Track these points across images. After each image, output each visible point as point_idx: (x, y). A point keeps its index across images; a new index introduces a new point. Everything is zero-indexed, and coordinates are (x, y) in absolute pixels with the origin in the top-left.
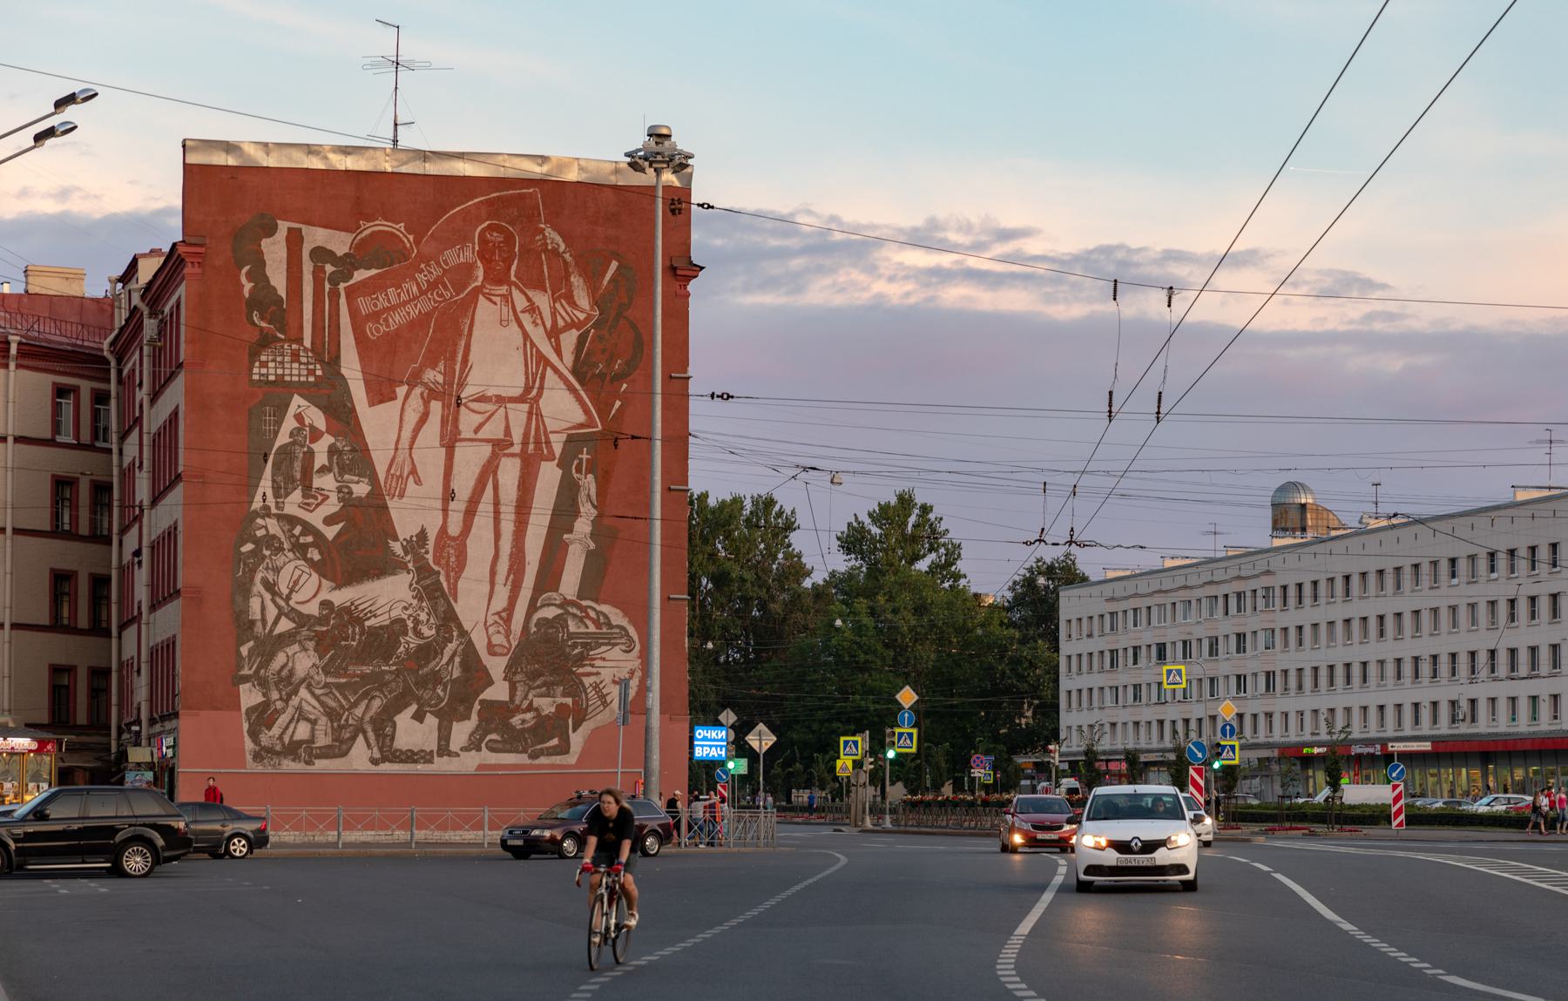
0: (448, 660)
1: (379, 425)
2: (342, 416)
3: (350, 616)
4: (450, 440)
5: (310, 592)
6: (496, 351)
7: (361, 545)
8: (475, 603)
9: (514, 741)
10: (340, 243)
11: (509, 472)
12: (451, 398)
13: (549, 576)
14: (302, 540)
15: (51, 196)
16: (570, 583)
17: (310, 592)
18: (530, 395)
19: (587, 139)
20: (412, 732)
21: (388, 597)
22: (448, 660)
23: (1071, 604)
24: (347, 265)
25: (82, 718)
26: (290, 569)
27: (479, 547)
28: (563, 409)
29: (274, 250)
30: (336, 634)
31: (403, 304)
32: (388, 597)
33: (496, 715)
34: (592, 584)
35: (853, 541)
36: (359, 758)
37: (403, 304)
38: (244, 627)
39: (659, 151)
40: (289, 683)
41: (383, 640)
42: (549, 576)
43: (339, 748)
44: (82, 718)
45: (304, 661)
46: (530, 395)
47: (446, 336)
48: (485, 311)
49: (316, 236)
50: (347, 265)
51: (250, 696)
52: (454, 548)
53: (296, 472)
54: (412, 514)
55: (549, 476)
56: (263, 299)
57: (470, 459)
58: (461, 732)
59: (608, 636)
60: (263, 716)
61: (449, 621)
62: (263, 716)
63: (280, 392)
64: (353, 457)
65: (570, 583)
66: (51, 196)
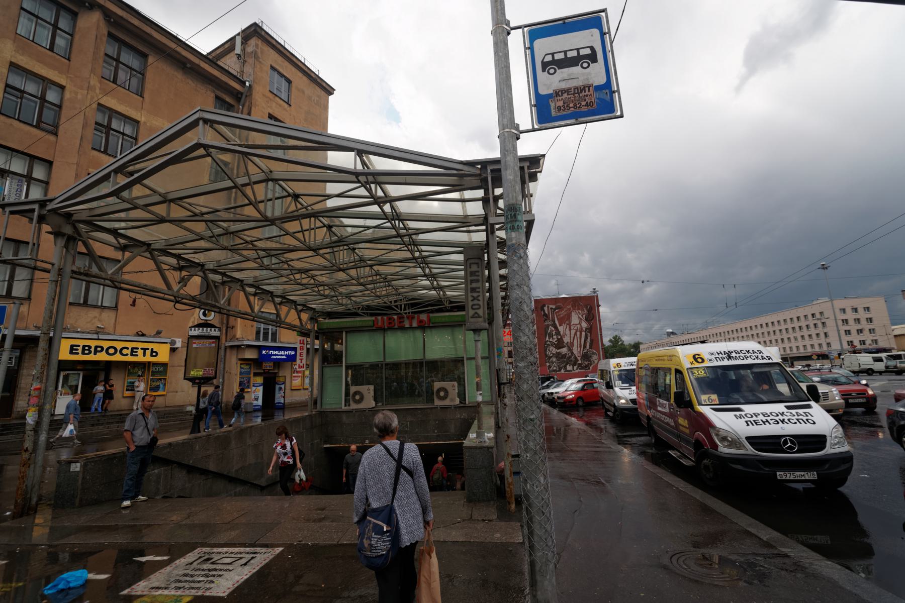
0: (573, 358)
1: (561, 329)
2: (556, 328)
3: (559, 353)
4: (570, 330)
5: (554, 351)
6: (575, 319)
7: (560, 344)
8: (576, 350)
9: (582, 368)
10: (554, 307)
11: (578, 333)
12: (569, 324)
13: (585, 347)
14: (552, 344)
15: (744, 80)
16: (588, 347)
17: (554, 351)
18: (580, 324)
19: (585, 292)
20: (569, 368)
21: (564, 350)
22: (573, 358)
23: (641, 347)
24: (555, 309)
25: (293, 353)
26: (551, 348)
27: (575, 343)
28: (584, 325)
29: (546, 308)
30: (558, 355)
31: (563, 313)
32: (564, 350)
33: (580, 365)
34: (591, 347)
35: (610, 341)
36: (563, 371)
37: (563, 313)
38: (546, 355)
39: (594, 291)
40: (552, 362)
41: (564, 356)
42: (585, 347)
43: (560, 370)
44: (293, 353)
45: (554, 360)
46: (580, 324)
47: (568, 317)
48: (573, 314)
49: (551, 306)
50: (555, 309)
51: (548, 364)
52: (572, 344)
53: (551, 336)
54: (566, 340)
55: (583, 333)
56: (545, 315)
57: (573, 332)
58: (575, 367)
59: (594, 354)
60: (550, 367)
61: (572, 353)
62: (550, 367)
63: (548, 326)
64: (558, 333)
65: (588, 347)
66: (744, 80)
